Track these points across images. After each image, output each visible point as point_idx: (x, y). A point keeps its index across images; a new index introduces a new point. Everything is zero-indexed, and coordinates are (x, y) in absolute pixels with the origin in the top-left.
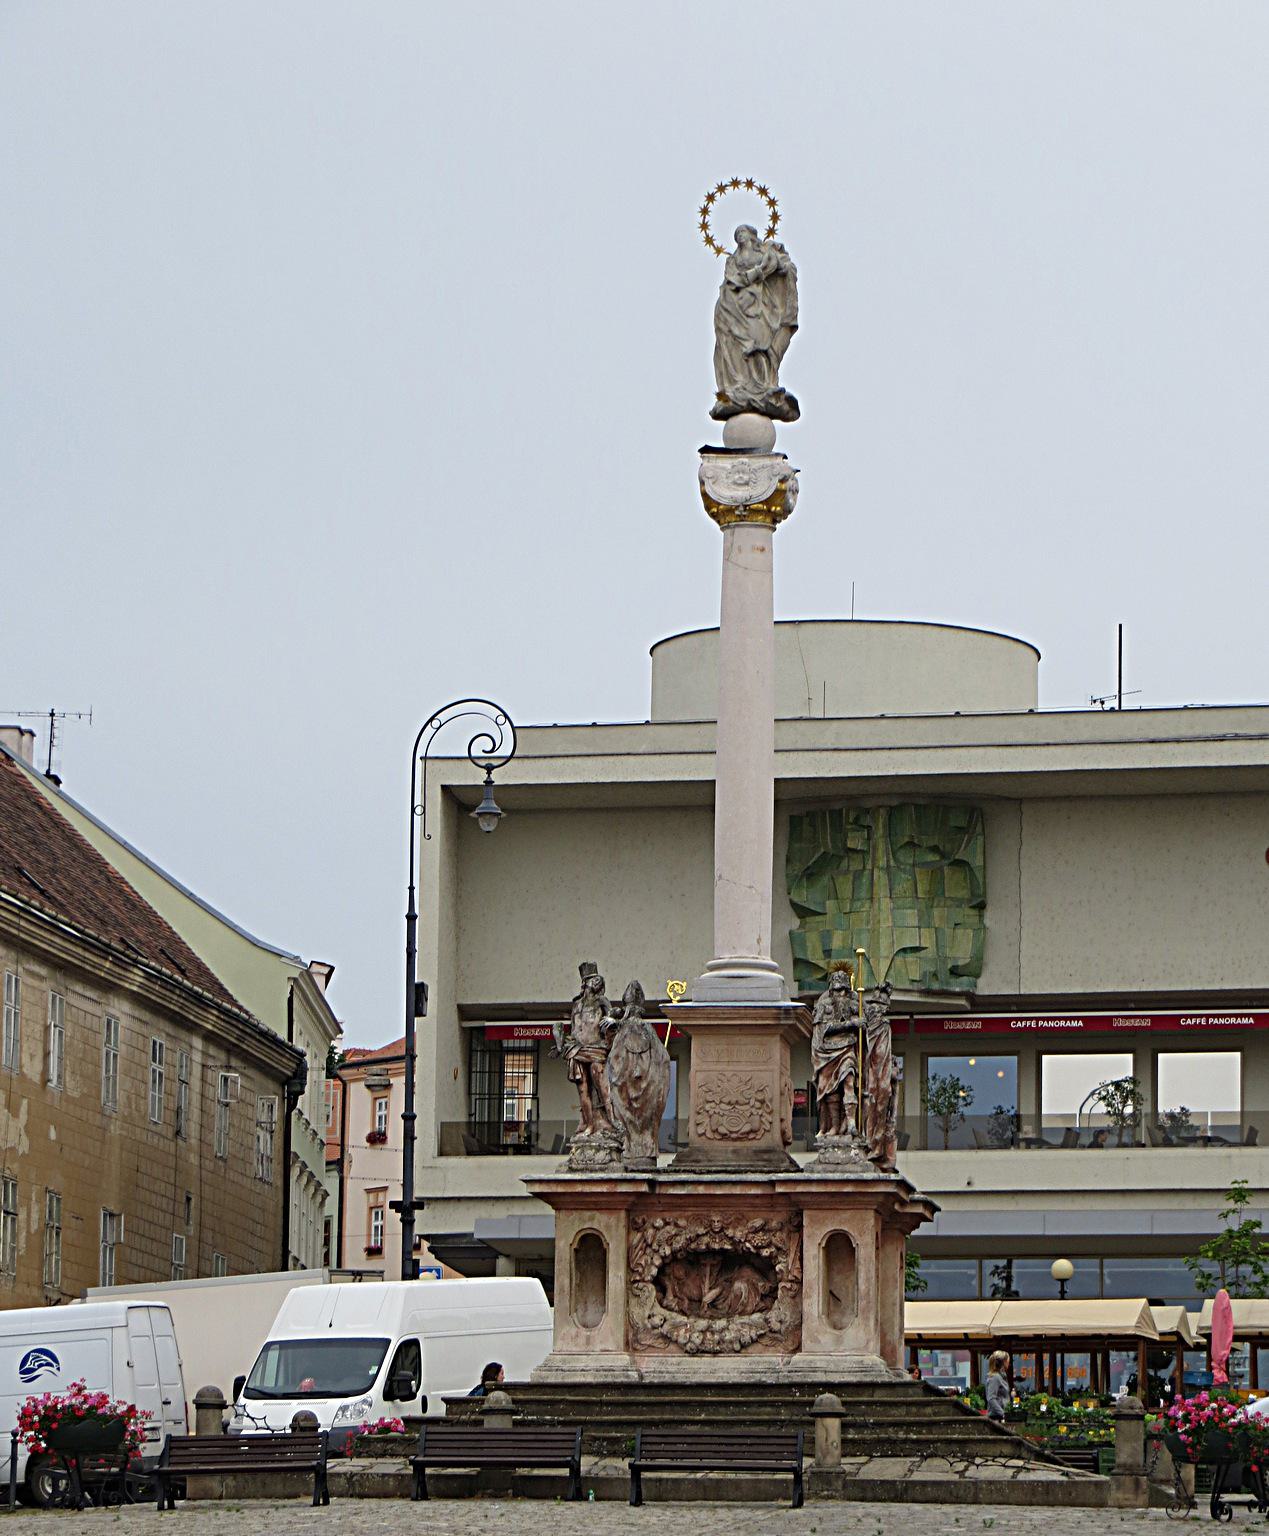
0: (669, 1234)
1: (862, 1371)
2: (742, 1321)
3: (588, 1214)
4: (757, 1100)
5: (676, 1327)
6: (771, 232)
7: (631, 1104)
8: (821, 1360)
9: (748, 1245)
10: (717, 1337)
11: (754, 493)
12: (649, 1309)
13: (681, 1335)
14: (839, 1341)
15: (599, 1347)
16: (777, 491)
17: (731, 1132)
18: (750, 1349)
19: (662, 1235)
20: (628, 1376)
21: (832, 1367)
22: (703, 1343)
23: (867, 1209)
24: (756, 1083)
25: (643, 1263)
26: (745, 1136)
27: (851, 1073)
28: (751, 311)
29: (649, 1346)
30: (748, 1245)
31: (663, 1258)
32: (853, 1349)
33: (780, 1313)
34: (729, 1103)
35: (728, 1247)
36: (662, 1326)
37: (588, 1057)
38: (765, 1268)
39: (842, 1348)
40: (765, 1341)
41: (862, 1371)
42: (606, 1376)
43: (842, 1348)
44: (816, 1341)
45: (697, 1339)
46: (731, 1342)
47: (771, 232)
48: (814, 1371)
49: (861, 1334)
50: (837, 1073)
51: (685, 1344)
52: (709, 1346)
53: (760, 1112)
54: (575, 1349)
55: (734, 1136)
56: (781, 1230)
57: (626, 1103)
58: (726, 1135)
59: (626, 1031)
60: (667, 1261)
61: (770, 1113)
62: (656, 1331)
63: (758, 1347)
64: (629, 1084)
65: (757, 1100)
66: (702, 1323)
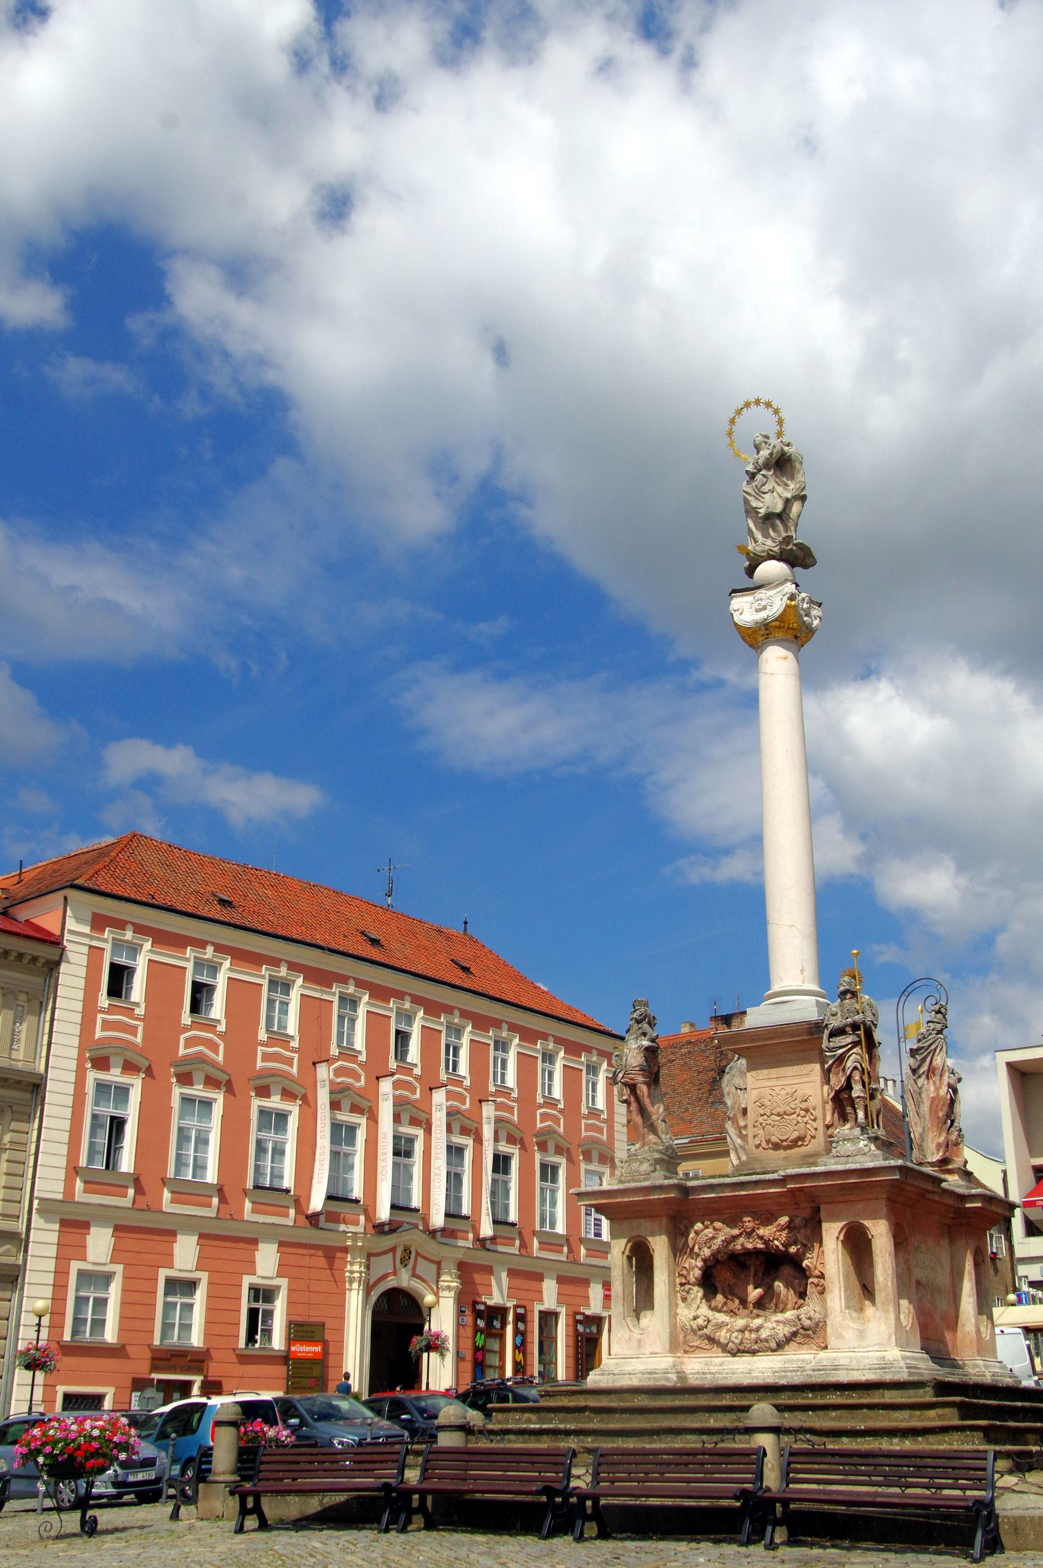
0: (709, 1237)
1: (882, 1368)
2: (777, 1319)
3: (635, 1222)
4: (801, 1109)
5: (720, 1326)
6: (780, 434)
7: (740, 1132)
8: (844, 1357)
9: (776, 1242)
10: (754, 1336)
11: (770, 613)
12: (696, 1309)
13: (723, 1335)
14: (861, 1334)
15: (648, 1350)
16: (787, 606)
17: (782, 1141)
18: (787, 1348)
19: (702, 1237)
20: (667, 1379)
21: (854, 1365)
22: (741, 1343)
23: (877, 1199)
24: (799, 1094)
25: (687, 1265)
26: (795, 1143)
27: (855, 1068)
28: (765, 489)
29: (697, 1347)
30: (776, 1242)
31: (705, 1261)
32: (878, 1344)
33: (811, 1308)
34: (778, 1115)
35: (760, 1246)
36: (706, 1327)
37: (632, 1079)
38: (795, 1263)
39: (865, 1344)
40: (799, 1339)
41: (882, 1368)
42: (649, 1379)
43: (865, 1344)
44: (840, 1337)
45: (736, 1337)
46: (767, 1341)
47: (780, 434)
48: (835, 1370)
49: (883, 1328)
50: (844, 1069)
51: (727, 1344)
52: (747, 1345)
53: (805, 1120)
54: (629, 1353)
55: (785, 1143)
56: (805, 1226)
57: (737, 1132)
58: (778, 1144)
59: (734, 1072)
60: (709, 1264)
61: (815, 1120)
62: (701, 1332)
63: (793, 1344)
64: (739, 1115)
65: (801, 1109)
66: (740, 1322)
